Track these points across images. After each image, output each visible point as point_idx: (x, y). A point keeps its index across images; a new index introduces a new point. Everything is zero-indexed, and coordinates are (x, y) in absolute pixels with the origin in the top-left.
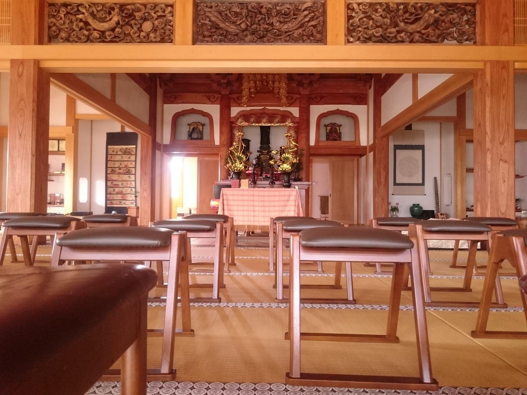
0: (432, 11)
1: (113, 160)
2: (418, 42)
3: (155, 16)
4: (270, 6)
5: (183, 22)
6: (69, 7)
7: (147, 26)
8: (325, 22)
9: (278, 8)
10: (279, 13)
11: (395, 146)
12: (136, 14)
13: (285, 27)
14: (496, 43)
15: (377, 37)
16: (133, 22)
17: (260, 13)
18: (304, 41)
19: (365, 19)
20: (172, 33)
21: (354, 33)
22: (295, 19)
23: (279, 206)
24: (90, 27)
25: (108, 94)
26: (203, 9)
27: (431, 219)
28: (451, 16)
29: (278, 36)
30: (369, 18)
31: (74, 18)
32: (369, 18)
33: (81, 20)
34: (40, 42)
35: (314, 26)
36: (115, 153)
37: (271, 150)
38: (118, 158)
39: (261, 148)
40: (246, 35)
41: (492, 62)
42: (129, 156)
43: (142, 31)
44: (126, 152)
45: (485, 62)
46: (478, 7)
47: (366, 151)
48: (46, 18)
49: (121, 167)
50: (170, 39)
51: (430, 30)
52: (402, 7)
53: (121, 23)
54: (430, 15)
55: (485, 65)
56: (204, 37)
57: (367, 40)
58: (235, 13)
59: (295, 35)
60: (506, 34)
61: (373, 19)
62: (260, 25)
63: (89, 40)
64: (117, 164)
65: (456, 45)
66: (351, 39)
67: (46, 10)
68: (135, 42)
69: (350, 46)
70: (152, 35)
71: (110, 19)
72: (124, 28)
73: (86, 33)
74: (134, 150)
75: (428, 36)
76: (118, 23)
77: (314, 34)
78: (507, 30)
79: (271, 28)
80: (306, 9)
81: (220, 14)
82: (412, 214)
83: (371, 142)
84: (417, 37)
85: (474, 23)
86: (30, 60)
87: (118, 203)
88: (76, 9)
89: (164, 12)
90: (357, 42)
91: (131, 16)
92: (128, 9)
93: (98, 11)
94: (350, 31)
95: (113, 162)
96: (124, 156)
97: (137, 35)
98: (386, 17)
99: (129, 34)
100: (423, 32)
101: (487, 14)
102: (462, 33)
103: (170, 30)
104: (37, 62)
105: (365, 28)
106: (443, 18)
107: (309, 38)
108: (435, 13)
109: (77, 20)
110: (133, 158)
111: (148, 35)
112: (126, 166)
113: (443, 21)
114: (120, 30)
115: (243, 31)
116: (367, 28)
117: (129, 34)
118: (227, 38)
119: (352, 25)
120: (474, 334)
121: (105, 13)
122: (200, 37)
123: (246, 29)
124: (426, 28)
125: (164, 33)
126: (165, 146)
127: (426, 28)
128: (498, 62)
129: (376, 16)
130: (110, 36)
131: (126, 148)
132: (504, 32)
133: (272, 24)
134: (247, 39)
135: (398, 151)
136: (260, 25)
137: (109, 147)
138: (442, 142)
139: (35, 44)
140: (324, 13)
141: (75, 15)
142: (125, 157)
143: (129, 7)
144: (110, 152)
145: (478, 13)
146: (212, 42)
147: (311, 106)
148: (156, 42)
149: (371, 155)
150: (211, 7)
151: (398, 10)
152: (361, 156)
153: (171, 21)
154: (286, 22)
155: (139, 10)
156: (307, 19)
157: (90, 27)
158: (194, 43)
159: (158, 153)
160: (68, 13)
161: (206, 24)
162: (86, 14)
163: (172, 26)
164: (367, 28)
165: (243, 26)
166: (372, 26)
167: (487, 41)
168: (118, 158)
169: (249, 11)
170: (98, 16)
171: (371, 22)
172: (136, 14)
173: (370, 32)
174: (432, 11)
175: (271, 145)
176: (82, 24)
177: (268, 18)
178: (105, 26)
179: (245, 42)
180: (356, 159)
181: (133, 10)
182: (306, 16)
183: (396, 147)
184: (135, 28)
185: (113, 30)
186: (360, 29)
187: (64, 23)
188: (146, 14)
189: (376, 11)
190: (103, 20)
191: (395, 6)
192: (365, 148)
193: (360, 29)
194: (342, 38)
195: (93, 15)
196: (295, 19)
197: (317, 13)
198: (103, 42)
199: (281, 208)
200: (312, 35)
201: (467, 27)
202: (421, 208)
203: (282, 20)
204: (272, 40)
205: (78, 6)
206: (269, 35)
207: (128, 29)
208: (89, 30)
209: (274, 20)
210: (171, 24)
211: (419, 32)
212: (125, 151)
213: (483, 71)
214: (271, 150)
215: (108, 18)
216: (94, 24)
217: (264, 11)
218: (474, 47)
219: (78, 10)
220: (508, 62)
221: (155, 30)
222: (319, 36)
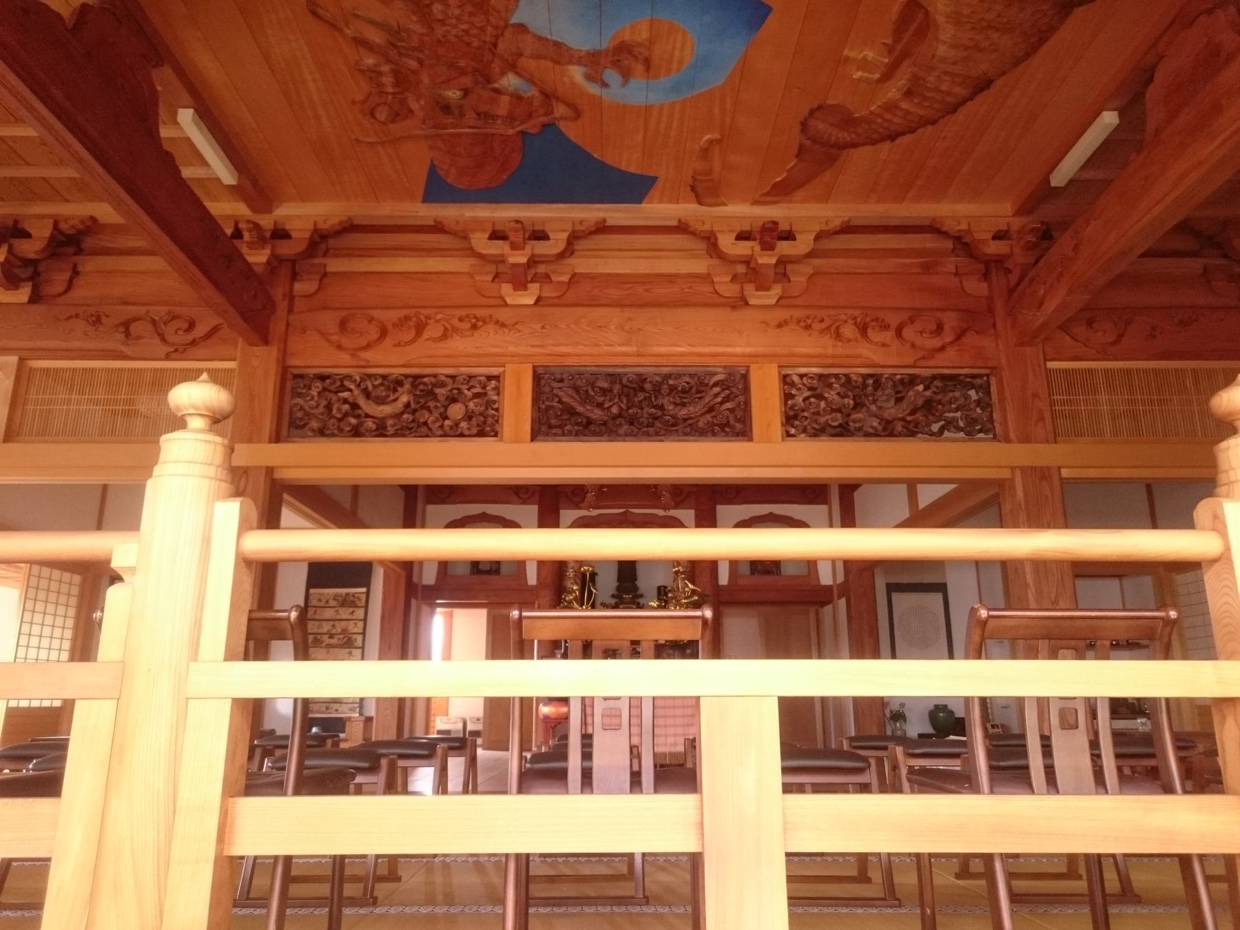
0: (921, 388)
1: (317, 617)
2: (900, 435)
3: (469, 394)
4: (658, 379)
5: (517, 405)
6: (328, 381)
7: (456, 411)
8: (748, 403)
9: (671, 382)
10: (672, 389)
11: (888, 585)
12: (438, 391)
13: (683, 412)
14: (1026, 439)
15: (835, 427)
16: (431, 404)
17: (642, 389)
18: (714, 434)
19: (812, 400)
20: (497, 421)
21: (794, 421)
22: (700, 398)
23: (684, 716)
24: (359, 412)
25: (347, 504)
26: (549, 384)
27: (952, 737)
28: (951, 395)
29: (673, 425)
30: (820, 397)
31: (334, 398)
32: (820, 397)
33: (345, 401)
34: (277, 438)
35: (732, 411)
36: (322, 604)
37: (639, 592)
38: (329, 613)
39: (618, 588)
40: (620, 425)
41: (1024, 469)
42: (351, 610)
43: (447, 418)
44: (347, 602)
45: (1013, 468)
46: (993, 381)
47: (832, 595)
48: (288, 396)
49: (334, 631)
50: (493, 430)
51: (918, 415)
52: (870, 381)
53: (413, 406)
54: (917, 393)
55: (1013, 474)
56: (550, 427)
57: (817, 433)
58: (602, 389)
59: (701, 424)
60: (1041, 424)
61: (825, 399)
62: (642, 409)
63: (356, 433)
64: (326, 627)
65: (963, 440)
66: (793, 431)
67: (289, 385)
68: (435, 436)
69: (791, 444)
70: (464, 424)
71: (395, 400)
72: (417, 414)
73: (353, 421)
74: (363, 597)
75: (916, 426)
76: (408, 405)
77: (732, 422)
78: (1042, 419)
79: (660, 413)
80: (716, 384)
81: (577, 391)
82: (935, 728)
83: (841, 578)
84: (899, 427)
85: (989, 405)
86: (260, 467)
87: (324, 709)
88: (338, 383)
89: (484, 387)
90: (803, 435)
91: (431, 394)
92: (425, 384)
93: (375, 387)
94: (791, 418)
95: (317, 623)
96: (342, 610)
97: (438, 424)
98: (847, 396)
99: (425, 423)
100: (909, 418)
101: (1007, 394)
102: (971, 422)
103: (493, 416)
104: (270, 470)
105: (814, 414)
106: (939, 397)
107: (723, 430)
108: (925, 389)
109: (339, 400)
110: (360, 613)
111: (457, 425)
112: (344, 631)
113: (939, 402)
114: (411, 418)
115: (615, 418)
116: (818, 413)
117: (425, 423)
118: (587, 429)
119: (792, 408)
120: (958, 876)
121: (388, 389)
122: (544, 428)
123: (620, 416)
124: (913, 413)
125: (485, 423)
126: (426, 587)
127: (913, 413)
128: (1033, 469)
129: (831, 395)
130: (393, 426)
131: (347, 594)
132: (1036, 424)
133: (662, 408)
134: (621, 431)
135: (895, 596)
136: (642, 409)
137: (312, 591)
138: (981, 576)
139: (270, 441)
140: (747, 389)
141: (336, 393)
142: (344, 613)
143: (426, 380)
144: (313, 602)
145: (993, 389)
146: (564, 435)
147: (719, 508)
148: (470, 436)
149: (842, 603)
150: (562, 381)
151: (865, 386)
152: (823, 604)
153: (495, 402)
154: (684, 405)
155: (443, 385)
156: (719, 400)
157: (359, 412)
158: (533, 438)
159: (414, 602)
160: (325, 389)
161: (552, 407)
162: (356, 392)
163: (497, 410)
164: (818, 413)
165: (615, 410)
166: (824, 410)
167: (1012, 436)
168: (329, 613)
169: (624, 386)
170: (374, 394)
171: (823, 404)
172: (438, 391)
173: (823, 420)
174: (921, 388)
175: (640, 583)
176: (347, 407)
177: (656, 397)
178: (386, 410)
179: (619, 435)
180: (812, 609)
181: (435, 385)
182: (716, 395)
183: (892, 588)
184: (436, 414)
185: (398, 416)
186: (805, 414)
187: (317, 406)
188: (455, 391)
189: (830, 386)
190: (381, 401)
191: (860, 380)
192: (828, 589)
193: (805, 414)
194: (777, 429)
195: (368, 395)
196: (700, 398)
197: (734, 390)
198: (382, 435)
199: (686, 720)
200: (728, 424)
201: (979, 410)
202: (952, 712)
203: (678, 401)
204: (663, 432)
205: (341, 380)
206: (658, 424)
207: (424, 416)
208: (358, 417)
209: (665, 401)
210: (496, 406)
211: (903, 419)
212: (345, 600)
213: (1012, 480)
214: (639, 592)
215: (392, 398)
216: (367, 407)
217: (648, 386)
218: (996, 445)
219: (342, 385)
220: (1049, 468)
221: (469, 417)
222: (739, 426)
